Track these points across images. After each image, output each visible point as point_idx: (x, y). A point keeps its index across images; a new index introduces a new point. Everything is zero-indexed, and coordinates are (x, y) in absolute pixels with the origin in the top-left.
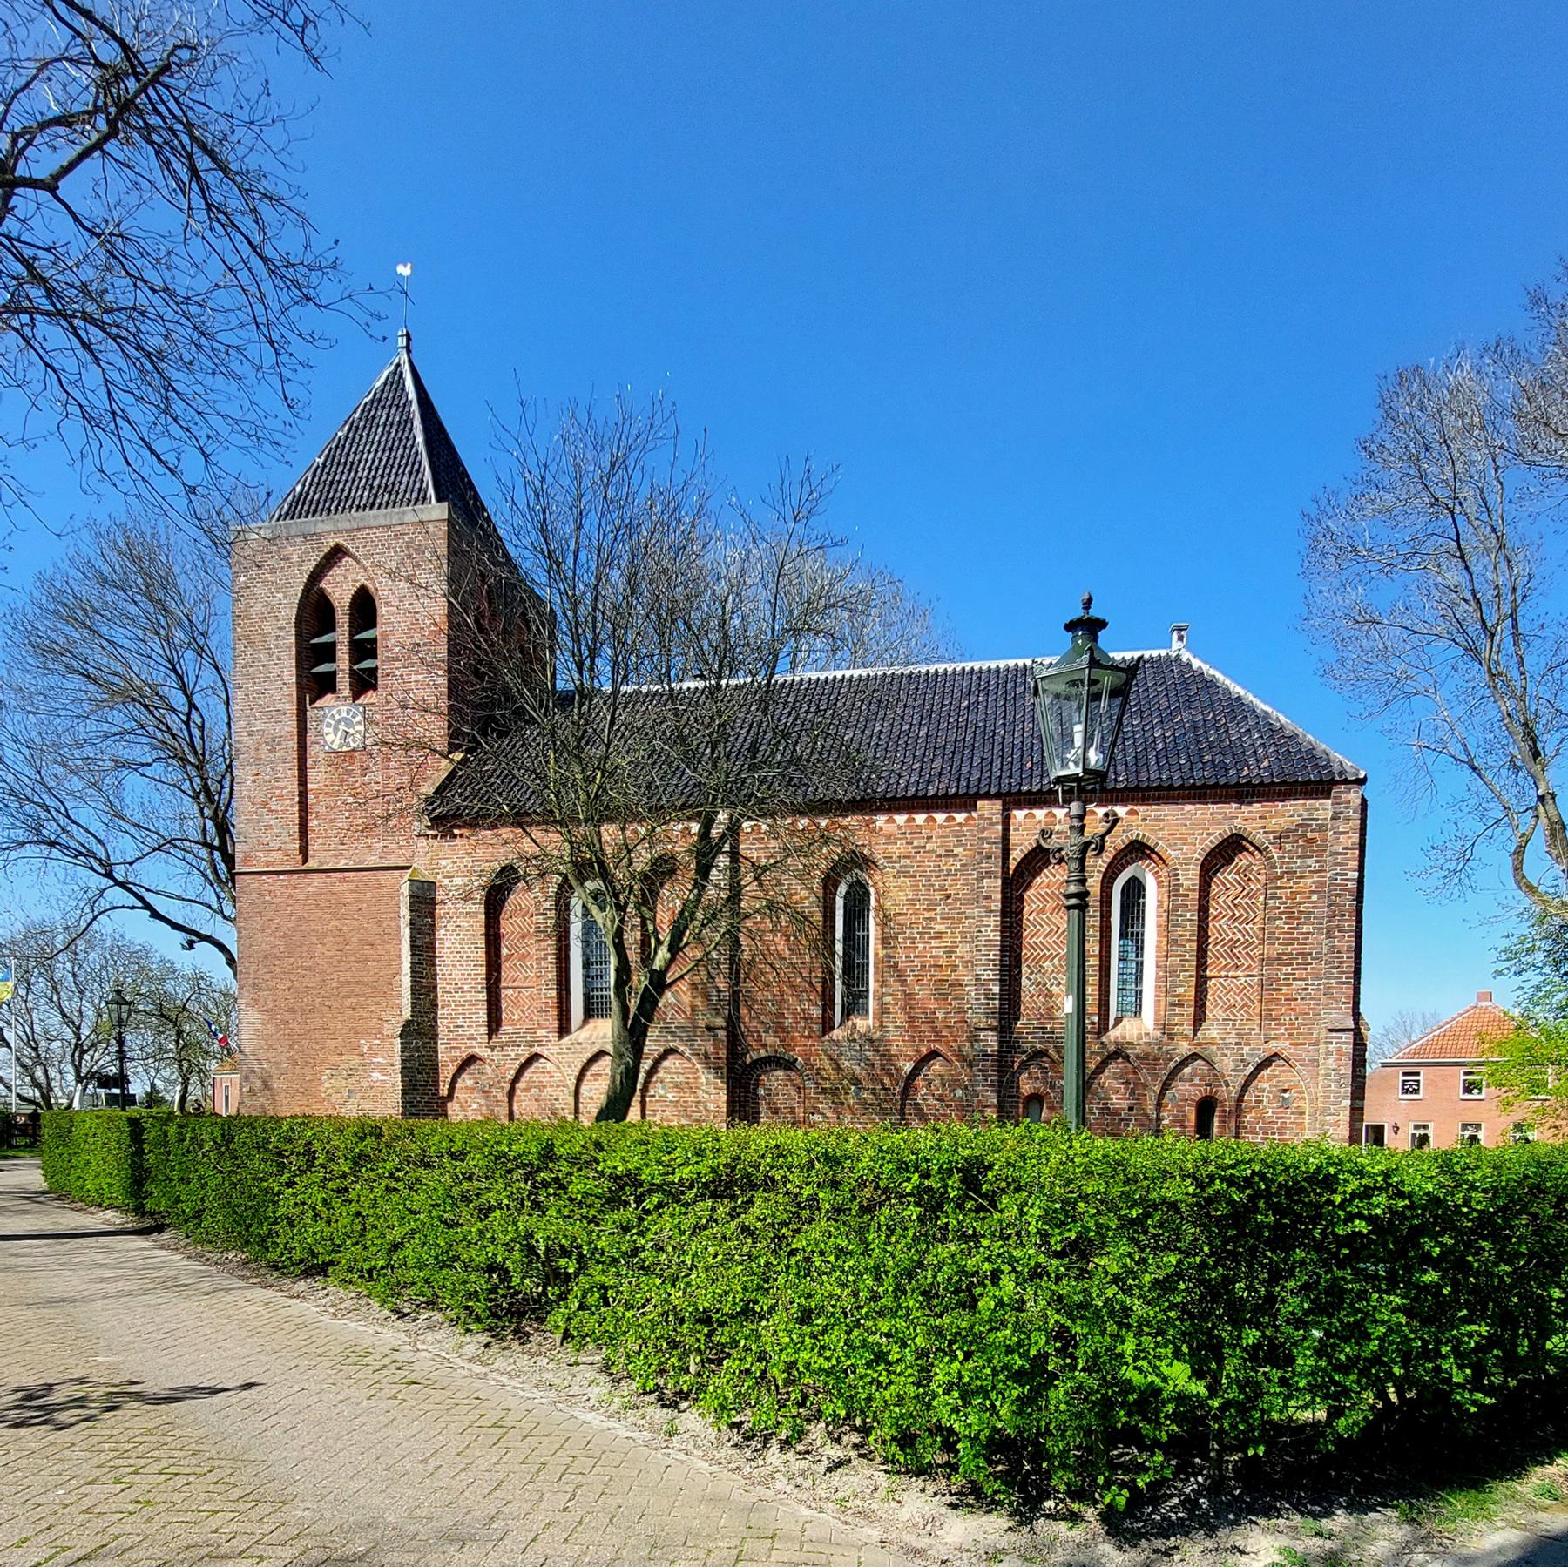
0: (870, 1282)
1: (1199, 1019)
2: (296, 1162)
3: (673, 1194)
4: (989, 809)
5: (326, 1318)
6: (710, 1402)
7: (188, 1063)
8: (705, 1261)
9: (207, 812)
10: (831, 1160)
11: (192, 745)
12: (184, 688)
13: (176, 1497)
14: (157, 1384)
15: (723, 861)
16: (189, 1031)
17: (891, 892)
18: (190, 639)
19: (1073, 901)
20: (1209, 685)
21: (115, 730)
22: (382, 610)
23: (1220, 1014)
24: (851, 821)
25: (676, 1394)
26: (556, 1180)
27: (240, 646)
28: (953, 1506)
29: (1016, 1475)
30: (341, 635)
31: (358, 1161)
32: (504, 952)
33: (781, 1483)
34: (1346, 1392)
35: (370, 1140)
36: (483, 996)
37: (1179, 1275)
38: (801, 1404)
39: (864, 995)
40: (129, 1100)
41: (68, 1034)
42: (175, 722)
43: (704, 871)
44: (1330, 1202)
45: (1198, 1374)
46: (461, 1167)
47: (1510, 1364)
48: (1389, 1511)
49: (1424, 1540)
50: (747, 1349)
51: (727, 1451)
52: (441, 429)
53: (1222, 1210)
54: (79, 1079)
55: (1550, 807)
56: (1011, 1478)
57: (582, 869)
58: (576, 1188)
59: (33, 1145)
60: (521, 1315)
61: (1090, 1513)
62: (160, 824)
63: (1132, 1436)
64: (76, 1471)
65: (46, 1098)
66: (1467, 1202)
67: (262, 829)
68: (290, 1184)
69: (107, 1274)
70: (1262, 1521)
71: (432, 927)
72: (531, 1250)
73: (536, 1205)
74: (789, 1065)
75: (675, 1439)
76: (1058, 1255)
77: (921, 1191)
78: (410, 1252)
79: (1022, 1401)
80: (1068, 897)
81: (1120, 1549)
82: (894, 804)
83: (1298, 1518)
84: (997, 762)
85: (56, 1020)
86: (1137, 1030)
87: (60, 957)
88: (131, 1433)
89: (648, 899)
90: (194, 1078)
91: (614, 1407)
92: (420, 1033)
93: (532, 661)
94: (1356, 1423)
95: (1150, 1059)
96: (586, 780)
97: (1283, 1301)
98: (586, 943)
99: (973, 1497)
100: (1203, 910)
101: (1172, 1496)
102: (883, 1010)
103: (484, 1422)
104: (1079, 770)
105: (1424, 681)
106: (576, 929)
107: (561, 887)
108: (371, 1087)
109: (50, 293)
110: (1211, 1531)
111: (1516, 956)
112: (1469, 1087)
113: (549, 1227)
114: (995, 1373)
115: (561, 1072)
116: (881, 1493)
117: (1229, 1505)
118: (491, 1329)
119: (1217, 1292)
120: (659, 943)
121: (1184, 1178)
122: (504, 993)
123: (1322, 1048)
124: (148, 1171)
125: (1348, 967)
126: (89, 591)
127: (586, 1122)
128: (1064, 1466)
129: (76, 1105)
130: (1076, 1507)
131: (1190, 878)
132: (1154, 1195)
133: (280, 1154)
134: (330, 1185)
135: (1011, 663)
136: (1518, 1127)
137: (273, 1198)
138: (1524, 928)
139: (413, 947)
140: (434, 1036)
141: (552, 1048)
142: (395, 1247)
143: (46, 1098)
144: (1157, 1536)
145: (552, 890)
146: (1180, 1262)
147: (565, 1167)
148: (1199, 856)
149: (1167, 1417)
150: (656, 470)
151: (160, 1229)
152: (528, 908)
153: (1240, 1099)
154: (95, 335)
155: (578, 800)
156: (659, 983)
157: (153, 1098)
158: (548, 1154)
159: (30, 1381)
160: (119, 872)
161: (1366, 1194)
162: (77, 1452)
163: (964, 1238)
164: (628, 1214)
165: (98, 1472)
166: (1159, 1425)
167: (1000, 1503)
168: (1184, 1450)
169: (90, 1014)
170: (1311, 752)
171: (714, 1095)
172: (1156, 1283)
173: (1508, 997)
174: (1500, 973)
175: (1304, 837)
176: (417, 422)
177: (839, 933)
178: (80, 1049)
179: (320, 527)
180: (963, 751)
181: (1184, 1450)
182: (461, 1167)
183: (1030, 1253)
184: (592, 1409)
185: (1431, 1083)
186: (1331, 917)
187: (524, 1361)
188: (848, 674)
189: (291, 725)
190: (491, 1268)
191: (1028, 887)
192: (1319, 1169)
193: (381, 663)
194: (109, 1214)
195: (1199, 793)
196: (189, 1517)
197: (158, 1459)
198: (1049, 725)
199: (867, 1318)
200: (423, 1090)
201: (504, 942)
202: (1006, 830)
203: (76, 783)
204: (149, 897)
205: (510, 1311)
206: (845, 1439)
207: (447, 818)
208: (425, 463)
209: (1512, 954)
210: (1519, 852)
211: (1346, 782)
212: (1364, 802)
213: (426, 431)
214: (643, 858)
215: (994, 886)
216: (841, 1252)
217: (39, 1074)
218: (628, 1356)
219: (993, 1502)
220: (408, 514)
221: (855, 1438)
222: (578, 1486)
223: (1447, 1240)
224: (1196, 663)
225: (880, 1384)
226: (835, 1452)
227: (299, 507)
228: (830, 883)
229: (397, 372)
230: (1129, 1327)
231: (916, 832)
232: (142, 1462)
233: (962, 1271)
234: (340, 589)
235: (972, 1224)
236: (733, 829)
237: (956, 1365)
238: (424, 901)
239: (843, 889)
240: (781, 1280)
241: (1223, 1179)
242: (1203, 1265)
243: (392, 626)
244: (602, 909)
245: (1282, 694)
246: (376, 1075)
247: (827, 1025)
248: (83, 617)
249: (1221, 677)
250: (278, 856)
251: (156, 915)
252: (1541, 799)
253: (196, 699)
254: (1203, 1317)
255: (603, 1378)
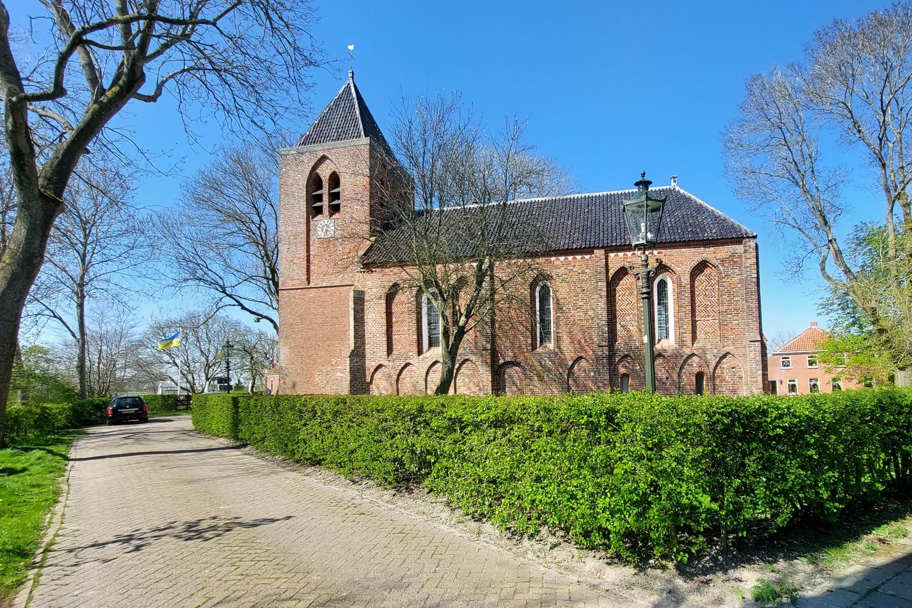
0: (567, 463)
1: (694, 339)
2: (307, 416)
3: (477, 426)
4: (599, 253)
5: (321, 485)
6: (496, 520)
7: (255, 373)
8: (492, 454)
9: (267, 264)
10: (548, 410)
11: (261, 237)
12: (258, 214)
13: (260, 572)
14: (248, 518)
15: (487, 278)
16: (256, 357)
17: (560, 289)
18: (257, 191)
19: (645, 296)
20: (688, 200)
21: (229, 231)
22: (342, 180)
23: (702, 336)
24: (541, 260)
25: (480, 515)
26: (425, 421)
27: (283, 196)
28: (608, 564)
29: (637, 549)
30: (325, 191)
31: (336, 414)
32: (394, 320)
33: (530, 555)
34: (778, 506)
35: (341, 405)
36: (385, 339)
37: (703, 456)
38: (538, 518)
39: (549, 333)
40: (229, 388)
41: (203, 359)
42: (254, 228)
43: (480, 283)
44: (765, 421)
45: (714, 500)
46: (382, 416)
47: (847, 488)
48: (802, 559)
49: (821, 571)
50: (513, 494)
51: (504, 541)
52: (366, 108)
53: (720, 427)
54: (207, 379)
55: (835, 245)
56: (633, 548)
57: (428, 284)
58: (434, 424)
59: (188, 409)
60: (408, 480)
61: (670, 565)
62: (247, 270)
63: (687, 529)
64: (214, 561)
65: (192, 387)
66: (823, 418)
67: (290, 270)
68: (305, 425)
69: (222, 467)
70: (747, 566)
71: (363, 310)
72: (413, 452)
73: (416, 432)
74: (518, 364)
75: (482, 536)
76: (651, 449)
77: (588, 423)
78: (359, 454)
79: (639, 515)
80: (643, 294)
81: (685, 581)
82: (558, 252)
83: (763, 564)
84: (601, 234)
85: (198, 354)
86: (668, 344)
87: (202, 327)
88: (237, 542)
89: (455, 296)
90: (258, 377)
91: (453, 522)
92: (358, 355)
93: (405, 199)
94: (785, 520)
95: (676, 355)
96: (429, 247)
97: (749, 466)
98: (429, 315)
99: (617, 559)
100: (692, 292)
101: (706, 556)
102: (558, 340)
103: (396, 531)
104: (644, 242)
105: (775, 195)
106: (424, 310)
107: (418, 291)
108: (335, 380)
109: (211, 62)
110: (725, 571)
111: (826, 306)
112: (811, 363)
113: (422, 442)
114: (625, 503)
115: (421, 371)
116: (576, 559)
117: (732, 559)
118: (395, 488)
119: (718, 463)
120: (461, 315)
121: (702, 413)
122: (394, 337)
123: (748, 349)
124: (240, 420)
125: (756, 314)
126: (219, 175)
127: (429, 392)
128: (658, 544)
129: (206, 390)
130: (664, 562)
131: (686, 280)
132: (690, 422)
133: (301, 412)
134: (323, 425)
135: (605, 193)
136: (834, 380)
137: (296, 431)
138: (828, 295)
139: (355, 319)
140: (364, 357)
141: (415, 360)
142: (352, 452)
143: (192, 387)
144: (701, 575)
145: (414, 293)
146: (704, 450)
147: (429, 415)
148: (689, 270)
149: (703, 520)
150: (454, 121)
151: (245, 446)
152: (404, 301)
153: (714, 372)
154: (230, 78)
155: (425, 255)
156: (462, 332)
157: (239, 386)
158: (421, 410)
159: (193, 519)
160: (228, 291)
161: (780, 417)
162: (213, 552)
163: (608, 442)
164: (458, 435)
165: (223, 561)
166: (699, 523)
167: (628, 562)
168: (711, 534)
169: (212, 349)
170: (733, 226)
171: (486, 376)
172: (693, 459)
173: (824, 323)
174: (820, 314)
175: (732, 260)
176: (357, 106)
177: (538, 308)
178: (208, 366)
179: (317, 148)
180: (590, 230)
181: (711, 534)
182: (382, 416)
183: (640, 449)
184: (443, 523)
185: (795, 362)
186: (747, 294)
187: (411, 502)
188: (537, 200)
189: (303, 228)
190: (395, 460)
191: (617, 285)
192: (760, 407)
193: (341, 201)
194: (222, 440)
195: (687, 244)
196: (266, 581)
197: (250, 554)
198: (630, 223)
199: (567, 479)
200: (360, 381)
201: (394, 315)
202: (607, 262)
203: (212, 253)
204: (242, 301)
205: (405, 479)
206: (557, 533)
207: (368, 264)
208: (360, 122)
209: (824, 306)
210: (824, 262)
211: (748, 237)
212: (757, 246)
213: (360, 109)
214: (453, 279)
215: (603, 285)
216: (553, 450)
217: (190, 377)
218: (458, 499)
219: (626, 561)
220: (356, 142)
221: (562, 533)
222: (440, 560)
223: (816, 435)
224: (682, 191)
225: (573, 509)
226: (553, 540)
227: (307, 140)
228: (532, 287)
229: (348, 87)
230: (683, 480)
231: (569, 264)
232: (243, 556)
233: (608, 457)
234: (324, 172)
235: (612, 437)
236: (491, 267)
237: (608, 499)
238: (359, 299)
239: (538, 289)
240: (527, 463)
241: (719, 413)
242: (713, 451)
243: (347, 186)
244: (436, 300)
245: (719, 203)
246: (339, 374)
247: (534, 347)
248: (216, 186)
249: (693, 197)
250: (298, 282)
251: (244, 308)
252: (830, 241)
253: (264, 218)
254: (715, 473)
255: (447, 509)
